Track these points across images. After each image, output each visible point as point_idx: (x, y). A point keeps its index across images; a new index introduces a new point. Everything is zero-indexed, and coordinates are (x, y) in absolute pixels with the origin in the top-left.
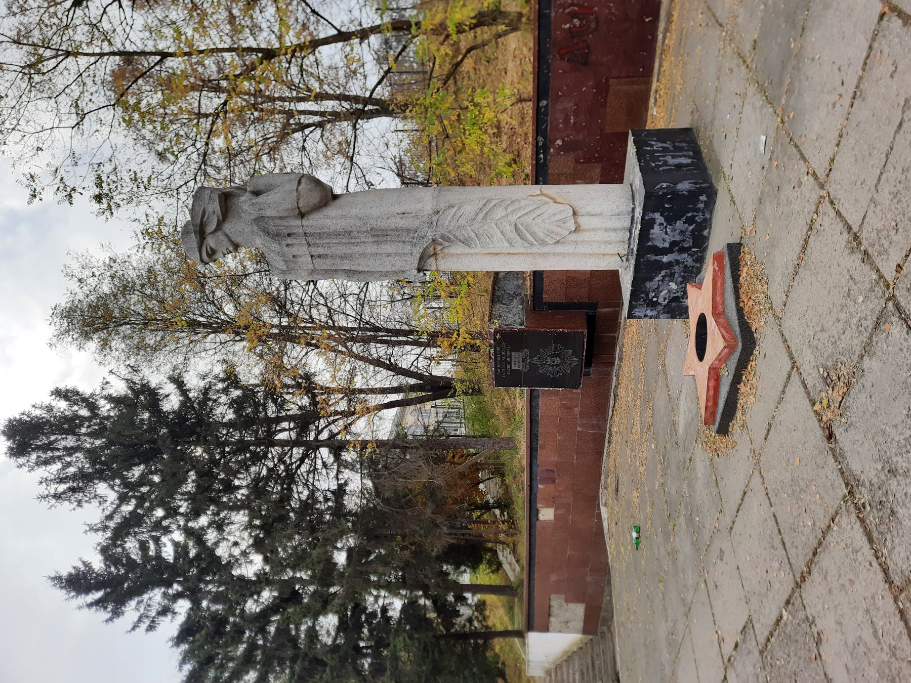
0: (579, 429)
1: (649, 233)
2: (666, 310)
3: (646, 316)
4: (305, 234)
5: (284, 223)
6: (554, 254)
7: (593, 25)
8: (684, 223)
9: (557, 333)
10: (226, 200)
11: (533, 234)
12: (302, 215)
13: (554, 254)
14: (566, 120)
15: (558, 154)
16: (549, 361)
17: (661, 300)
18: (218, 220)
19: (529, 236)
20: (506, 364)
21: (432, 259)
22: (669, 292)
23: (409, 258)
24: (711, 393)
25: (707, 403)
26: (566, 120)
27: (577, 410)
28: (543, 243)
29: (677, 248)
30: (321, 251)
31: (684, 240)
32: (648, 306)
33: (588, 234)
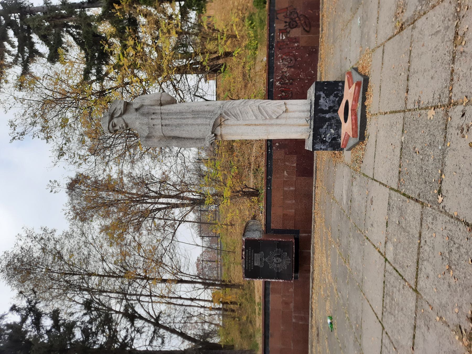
0: (294, 320)
1: (318, 102)
2: (330, 145)
3: (321, 149)
4: (161, 113)
5: (153, 107)
6: (277, 125)
7: (290, 95)
8: (334, 97)
9: (278, 241)
10: (127, 105)
11: (266, 112)
12: (161, 105)
13: (277, 125)
16: (275, 260)
18: (121, 113)
19: (265, 113)
20: (251, 261)
21: (219, 127)
22: (331, 134)
23: (208, 127)
24: (354, 121)
25: (352, 127)
27: (292, 305)
28: (271, 118)
29: (332, 110)
30: (167, 122)
32: (321, 143)
33: (291, 113)
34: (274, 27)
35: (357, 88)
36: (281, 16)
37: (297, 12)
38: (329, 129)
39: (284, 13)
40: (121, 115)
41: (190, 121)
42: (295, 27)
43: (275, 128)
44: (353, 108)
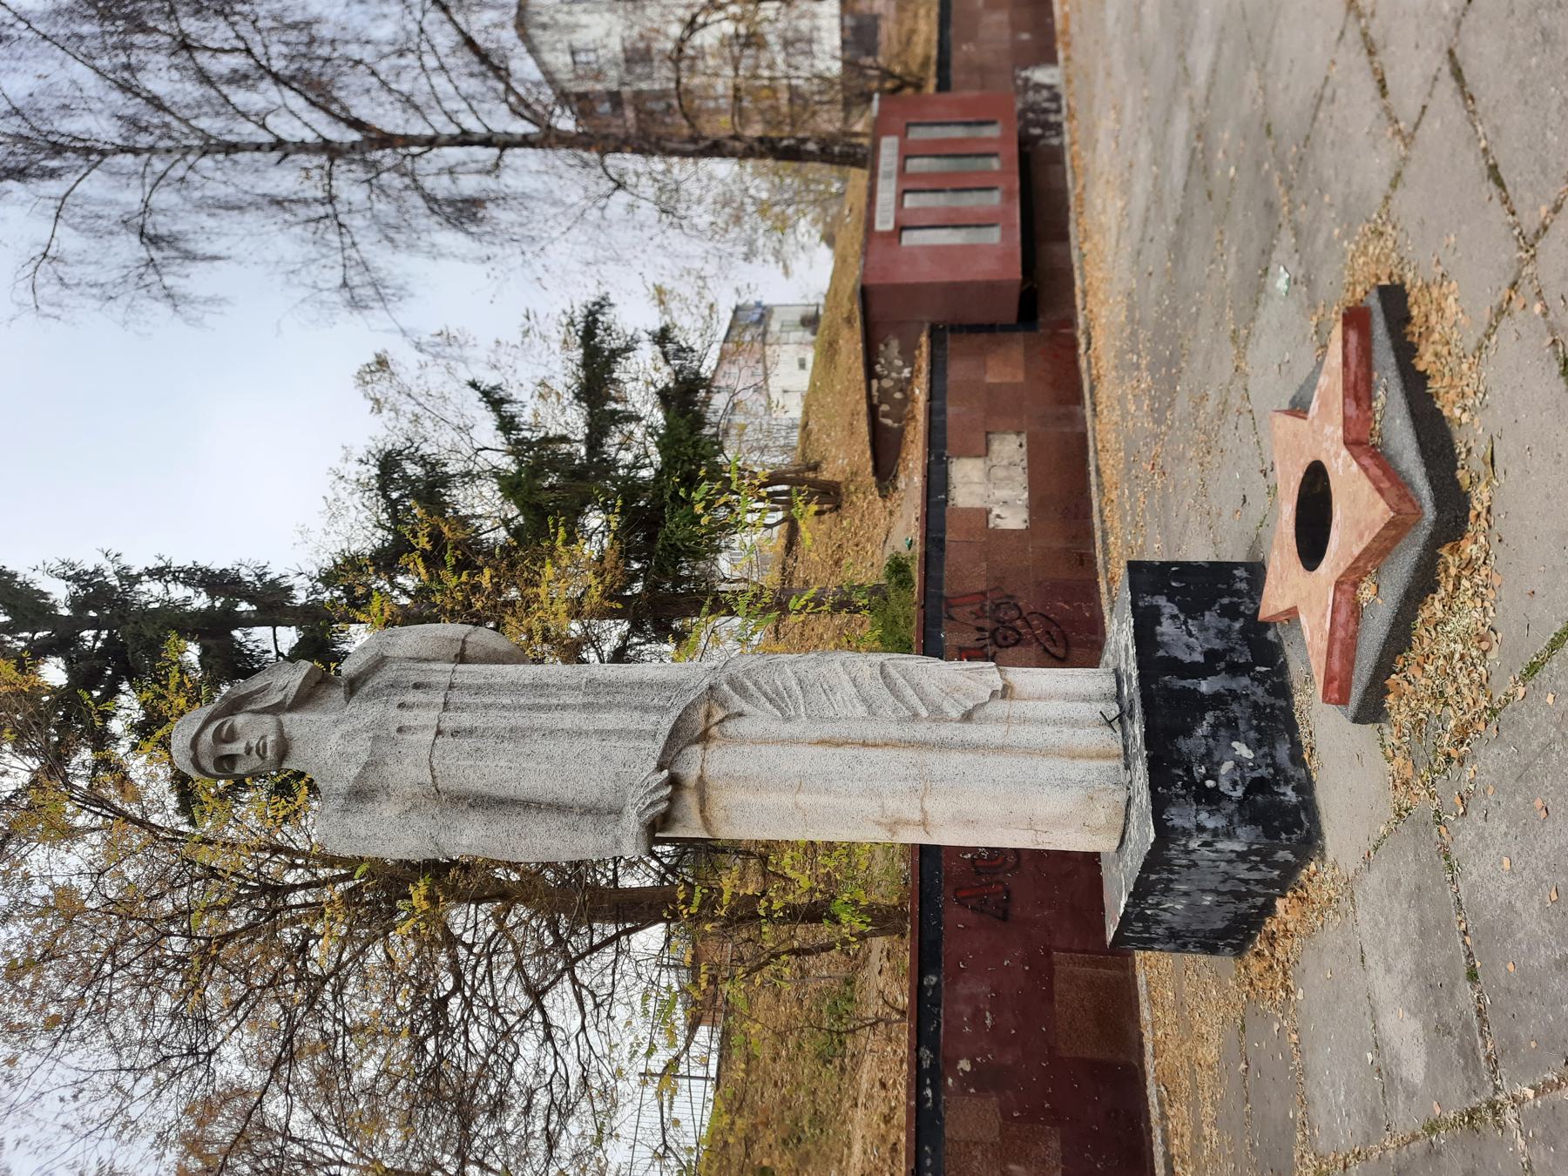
5: (425, 666)
6: (965, 746)
10: (318, 683)
11: (916, 688)
12: (462, 658)
13: (965, 746)
14: (977, 1017)
15: (965, 1092)
17: (1225, 786)
19: (909, 692)
21: (697, 748)
23: (647, 744)
26: (977, 1017)
28: (938, 715)
29: (1222, 665)
30: (465, 719)
31: (1233, 650)
32: (1198, 802)
34: (941, 641)
35: (1353, 337)
36: (963, 613)
37: (1016, 606)
38: (1223, 742)
39: (973, 604)
40: (276, 709)
41: (569, 720)
42: (1014, 645)
43: (956, 758)
44: (1353, 436)
